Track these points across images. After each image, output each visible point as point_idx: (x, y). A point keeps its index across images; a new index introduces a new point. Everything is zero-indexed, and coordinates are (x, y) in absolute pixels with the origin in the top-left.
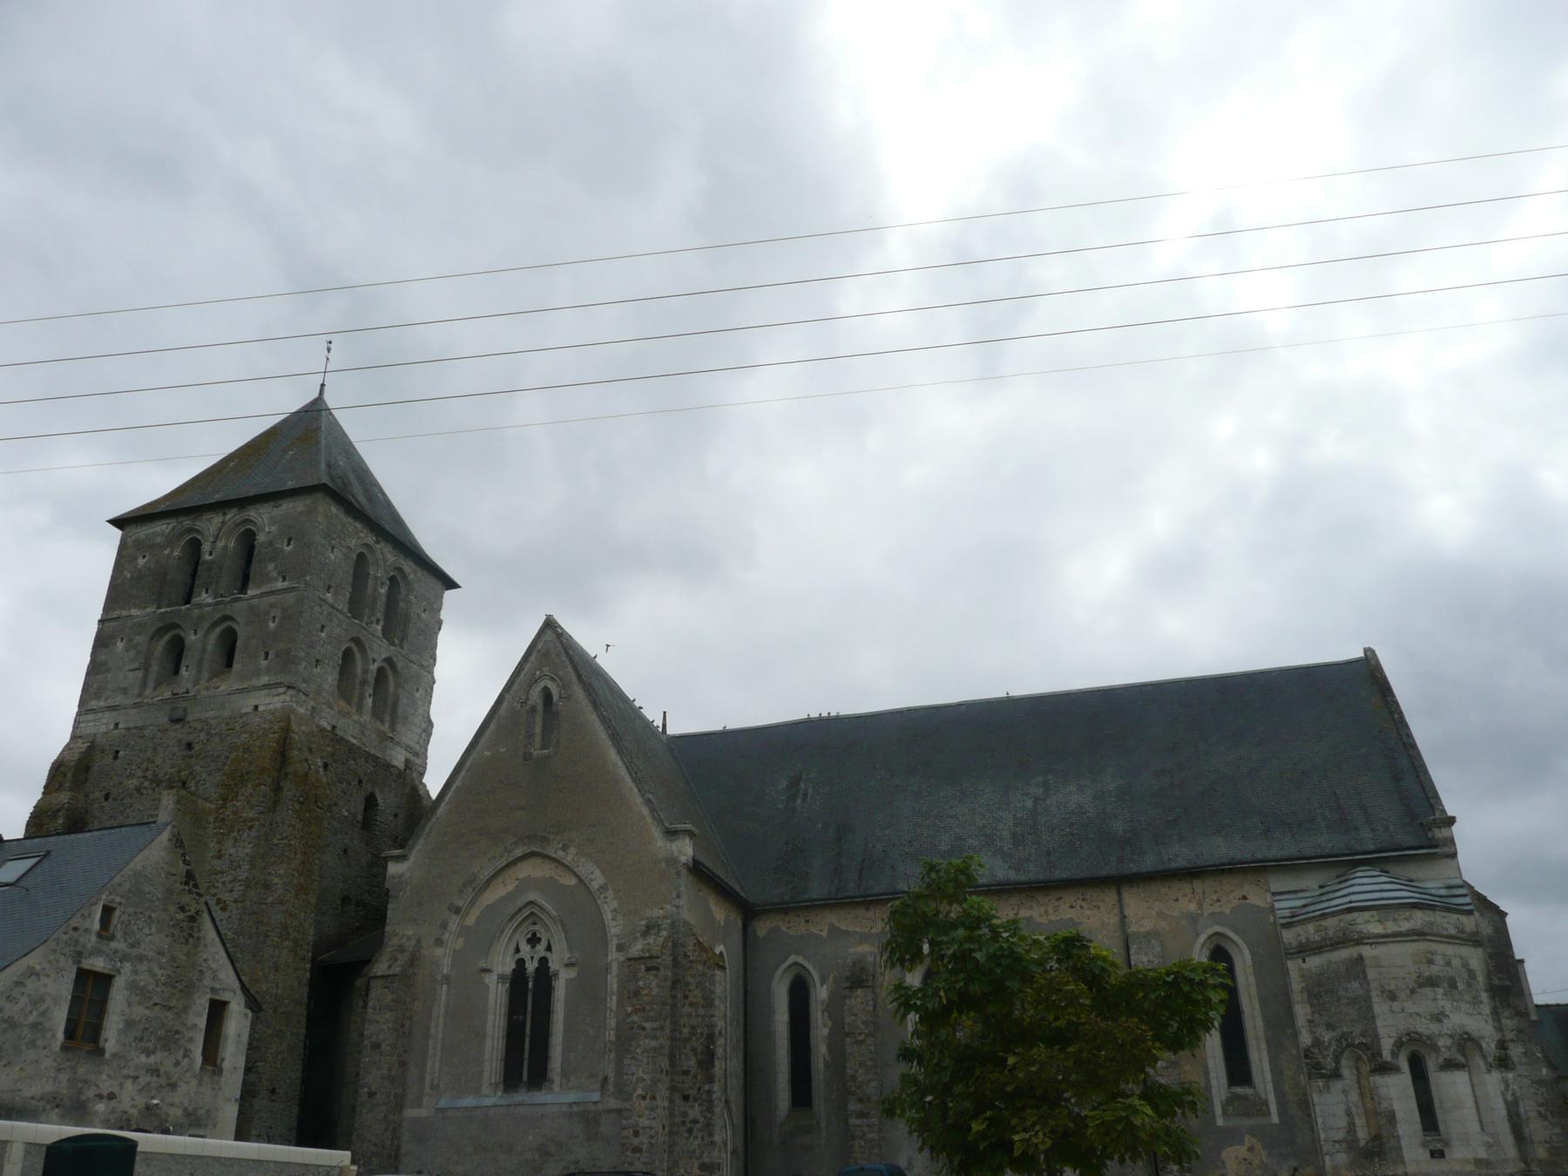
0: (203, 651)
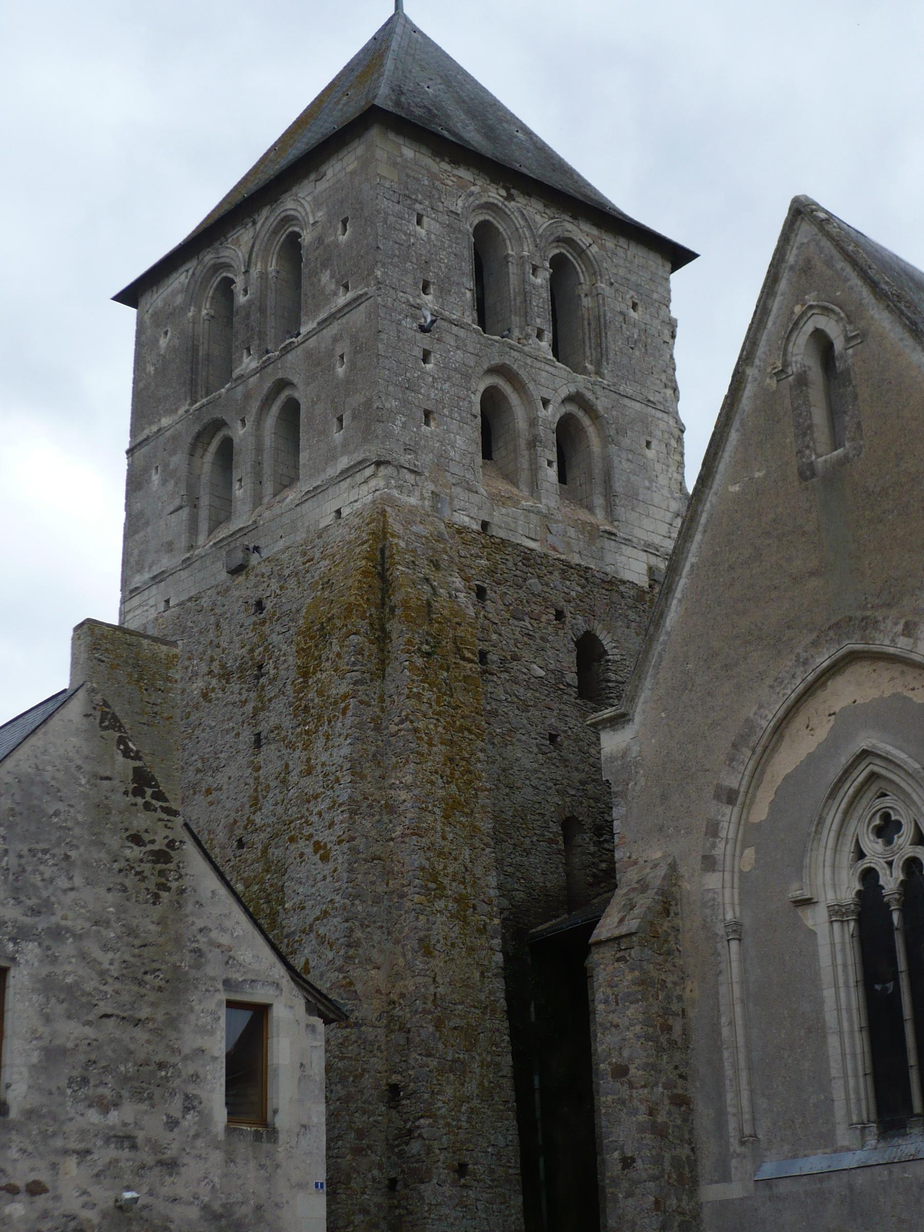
0: (259, 450)
